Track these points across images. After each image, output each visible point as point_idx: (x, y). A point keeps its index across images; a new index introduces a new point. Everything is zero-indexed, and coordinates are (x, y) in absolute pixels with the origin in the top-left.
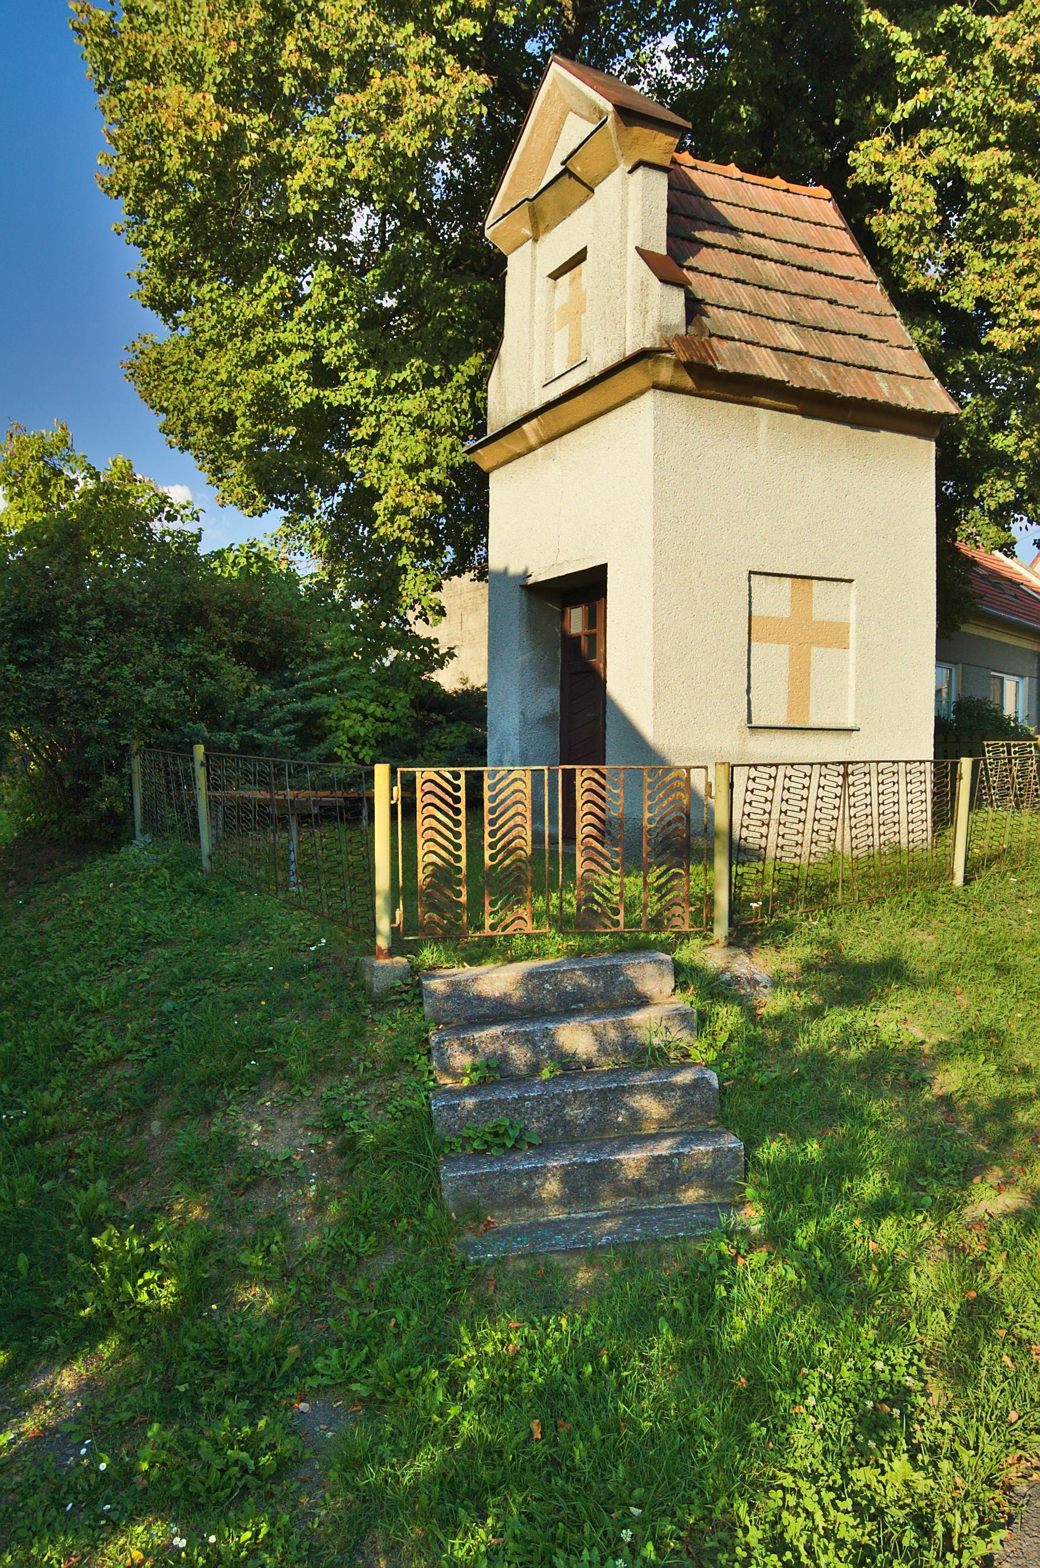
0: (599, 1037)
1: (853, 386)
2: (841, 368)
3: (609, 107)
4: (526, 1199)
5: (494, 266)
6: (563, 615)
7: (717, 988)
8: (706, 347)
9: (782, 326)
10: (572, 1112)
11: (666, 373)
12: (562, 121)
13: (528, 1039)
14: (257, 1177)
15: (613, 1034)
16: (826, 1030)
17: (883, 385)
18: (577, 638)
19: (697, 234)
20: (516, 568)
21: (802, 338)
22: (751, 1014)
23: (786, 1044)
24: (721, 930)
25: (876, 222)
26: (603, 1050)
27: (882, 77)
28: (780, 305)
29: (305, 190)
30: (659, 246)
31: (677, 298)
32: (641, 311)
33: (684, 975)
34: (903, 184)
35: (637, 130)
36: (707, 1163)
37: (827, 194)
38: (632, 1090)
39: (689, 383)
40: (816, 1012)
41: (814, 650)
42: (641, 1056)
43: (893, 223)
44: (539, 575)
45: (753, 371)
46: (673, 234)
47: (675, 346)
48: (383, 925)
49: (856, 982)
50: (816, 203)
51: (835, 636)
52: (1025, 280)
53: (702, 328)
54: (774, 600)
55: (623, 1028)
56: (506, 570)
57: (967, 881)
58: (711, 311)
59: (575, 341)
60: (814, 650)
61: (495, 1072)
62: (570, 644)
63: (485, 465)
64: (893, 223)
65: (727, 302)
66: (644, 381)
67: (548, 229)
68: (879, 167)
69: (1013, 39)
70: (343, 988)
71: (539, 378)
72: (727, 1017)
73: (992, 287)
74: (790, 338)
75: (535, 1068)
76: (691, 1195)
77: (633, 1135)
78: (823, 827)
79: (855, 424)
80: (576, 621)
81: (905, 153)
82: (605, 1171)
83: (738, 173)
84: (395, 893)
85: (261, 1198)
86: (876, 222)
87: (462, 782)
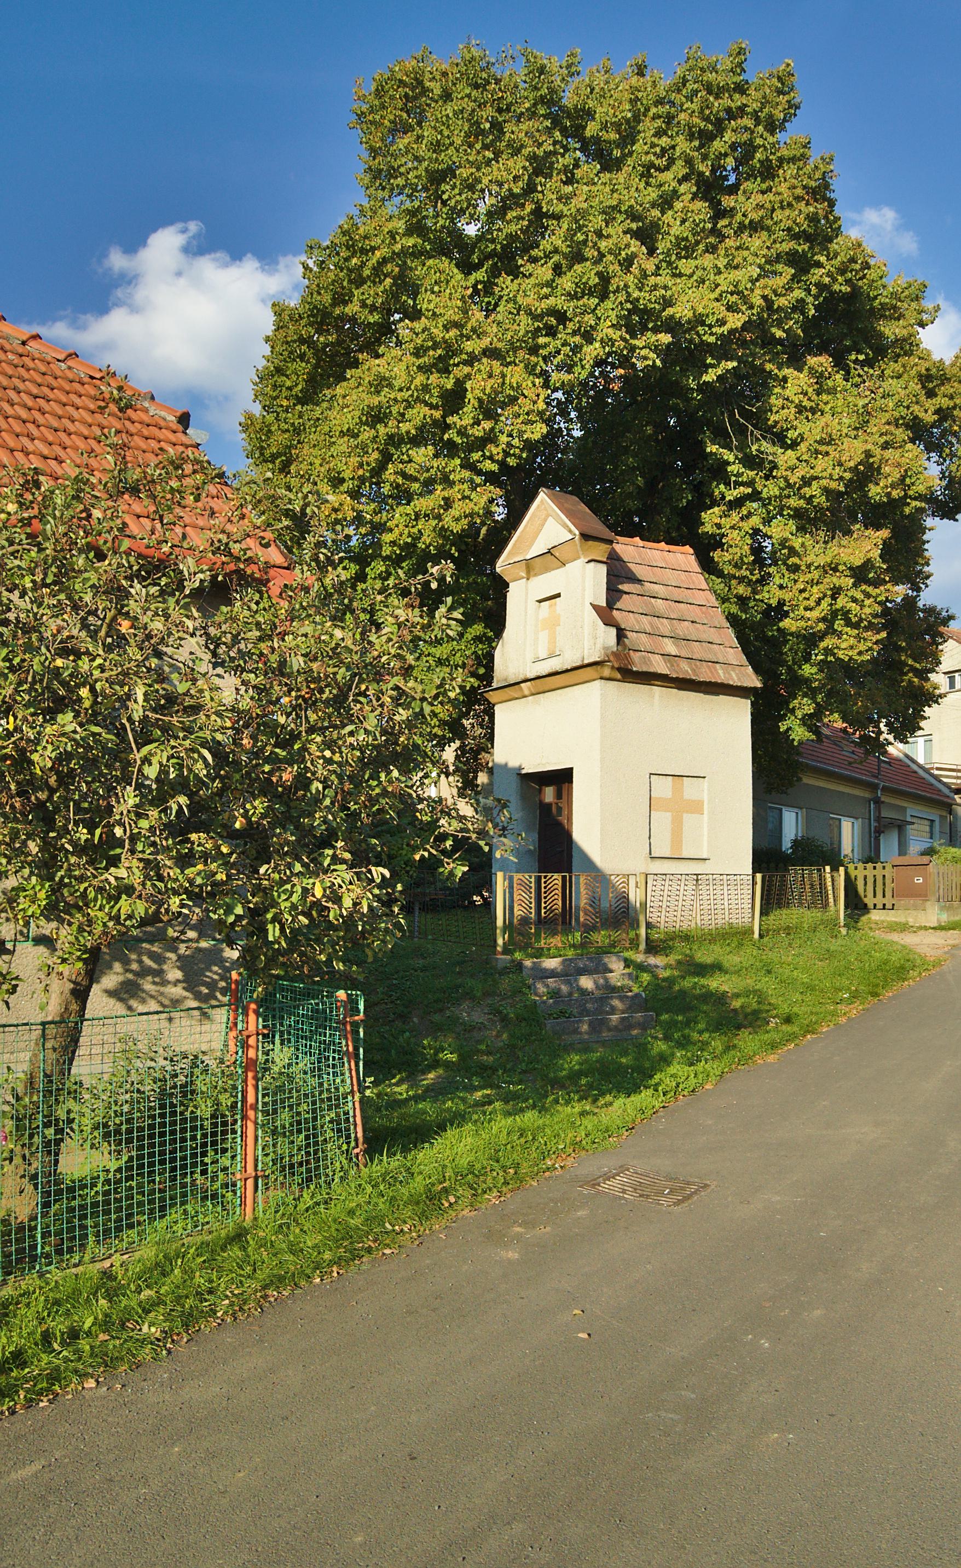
0: (595, 982)
1: (705, 674)
2: (698, 663)
3: (577, 532)
4: (576, 1031)
5: (501, 586)
6: (540, 791)
7: (641, 967)
8: (627, 657)
9: (666, 640)
10: (589, 1006)
11: (607, 672)
12: (545, 520)
13: (568, 983)
14: (470, 1028)
15: (602, 981)
16: (688, 983)
17: (721, 672)
18: (550, 805)
19: (620, 587)
20: (513, 763)
21: (677, 646)
22: (655, 976)
23: (670, 988)
24: (642, 946)
25: (716, 555)
26: (597, 987)
27: (719, 471)
28: (664, 626)
29: (393, 543)
30: (603, 603)
31: (613, 631)
32: (596, 640)
33: (628, 963)
34: (733, 537)
35: (590, 543)
36: (641, 1020)
37: (691, 551)
38: (612, 998)
39: (619, 676)
40: (683, 978)
41: (685, 815)
42: (611, 990)
43: (727, 557)
44: (528, 769)
45: (652, 670)
46: (609, 589)
47: (612, 658)
48: (500, 941)
49: (702, 970)
50: (685, 557)
51: (696, 807)
52: (804, 595)
53: (625, 645)
54: (663, 788)
55: (606, 980)
56: (506, 764)
57: (761, 936)
58: (629, 634)
59: (552, 640)
60: (685, 815)
61: (555, 994)
62: (545, 809)
63: (492, 700)
64: (727, 557)
65: (637, 628)
66: (596, 675)
67: (536, 575)
68: (719, 526)
69: (792, 469)
70: (485, 966)
71: (530, 657)
72: (646, 977)
73: (787, 596)
74: (671, 648)
75: (570, 994)
76: (635, 1032)
77: (613, 1010)
78: (687, 903)
79: (706, 692)
80: (549, 794)
81: (735, 517)
82: (603, 1022)
83: (641, 543)
84: (505, 928)
85: (475, 1034)
86: (716, 555)
87: (533, 880)
